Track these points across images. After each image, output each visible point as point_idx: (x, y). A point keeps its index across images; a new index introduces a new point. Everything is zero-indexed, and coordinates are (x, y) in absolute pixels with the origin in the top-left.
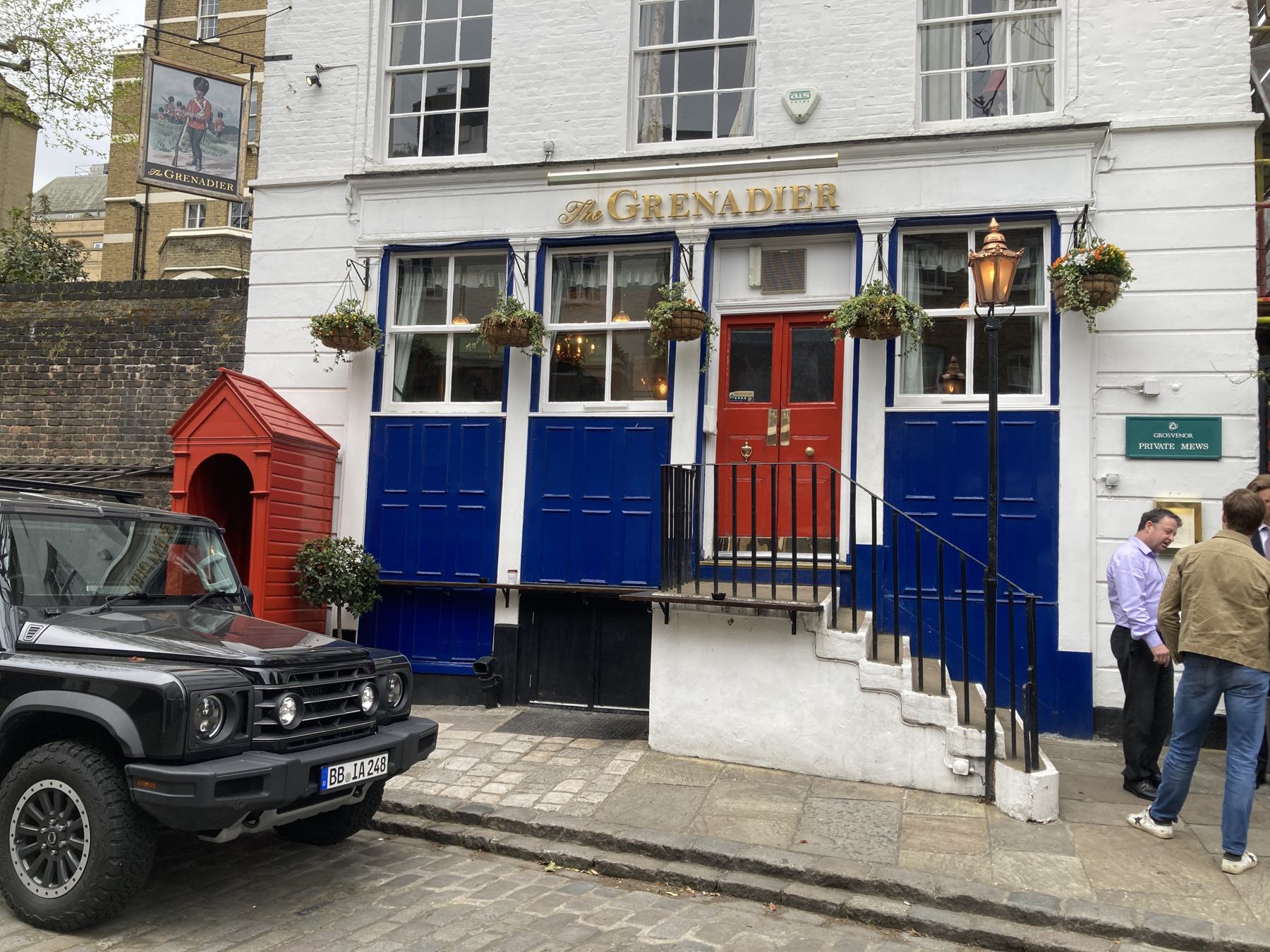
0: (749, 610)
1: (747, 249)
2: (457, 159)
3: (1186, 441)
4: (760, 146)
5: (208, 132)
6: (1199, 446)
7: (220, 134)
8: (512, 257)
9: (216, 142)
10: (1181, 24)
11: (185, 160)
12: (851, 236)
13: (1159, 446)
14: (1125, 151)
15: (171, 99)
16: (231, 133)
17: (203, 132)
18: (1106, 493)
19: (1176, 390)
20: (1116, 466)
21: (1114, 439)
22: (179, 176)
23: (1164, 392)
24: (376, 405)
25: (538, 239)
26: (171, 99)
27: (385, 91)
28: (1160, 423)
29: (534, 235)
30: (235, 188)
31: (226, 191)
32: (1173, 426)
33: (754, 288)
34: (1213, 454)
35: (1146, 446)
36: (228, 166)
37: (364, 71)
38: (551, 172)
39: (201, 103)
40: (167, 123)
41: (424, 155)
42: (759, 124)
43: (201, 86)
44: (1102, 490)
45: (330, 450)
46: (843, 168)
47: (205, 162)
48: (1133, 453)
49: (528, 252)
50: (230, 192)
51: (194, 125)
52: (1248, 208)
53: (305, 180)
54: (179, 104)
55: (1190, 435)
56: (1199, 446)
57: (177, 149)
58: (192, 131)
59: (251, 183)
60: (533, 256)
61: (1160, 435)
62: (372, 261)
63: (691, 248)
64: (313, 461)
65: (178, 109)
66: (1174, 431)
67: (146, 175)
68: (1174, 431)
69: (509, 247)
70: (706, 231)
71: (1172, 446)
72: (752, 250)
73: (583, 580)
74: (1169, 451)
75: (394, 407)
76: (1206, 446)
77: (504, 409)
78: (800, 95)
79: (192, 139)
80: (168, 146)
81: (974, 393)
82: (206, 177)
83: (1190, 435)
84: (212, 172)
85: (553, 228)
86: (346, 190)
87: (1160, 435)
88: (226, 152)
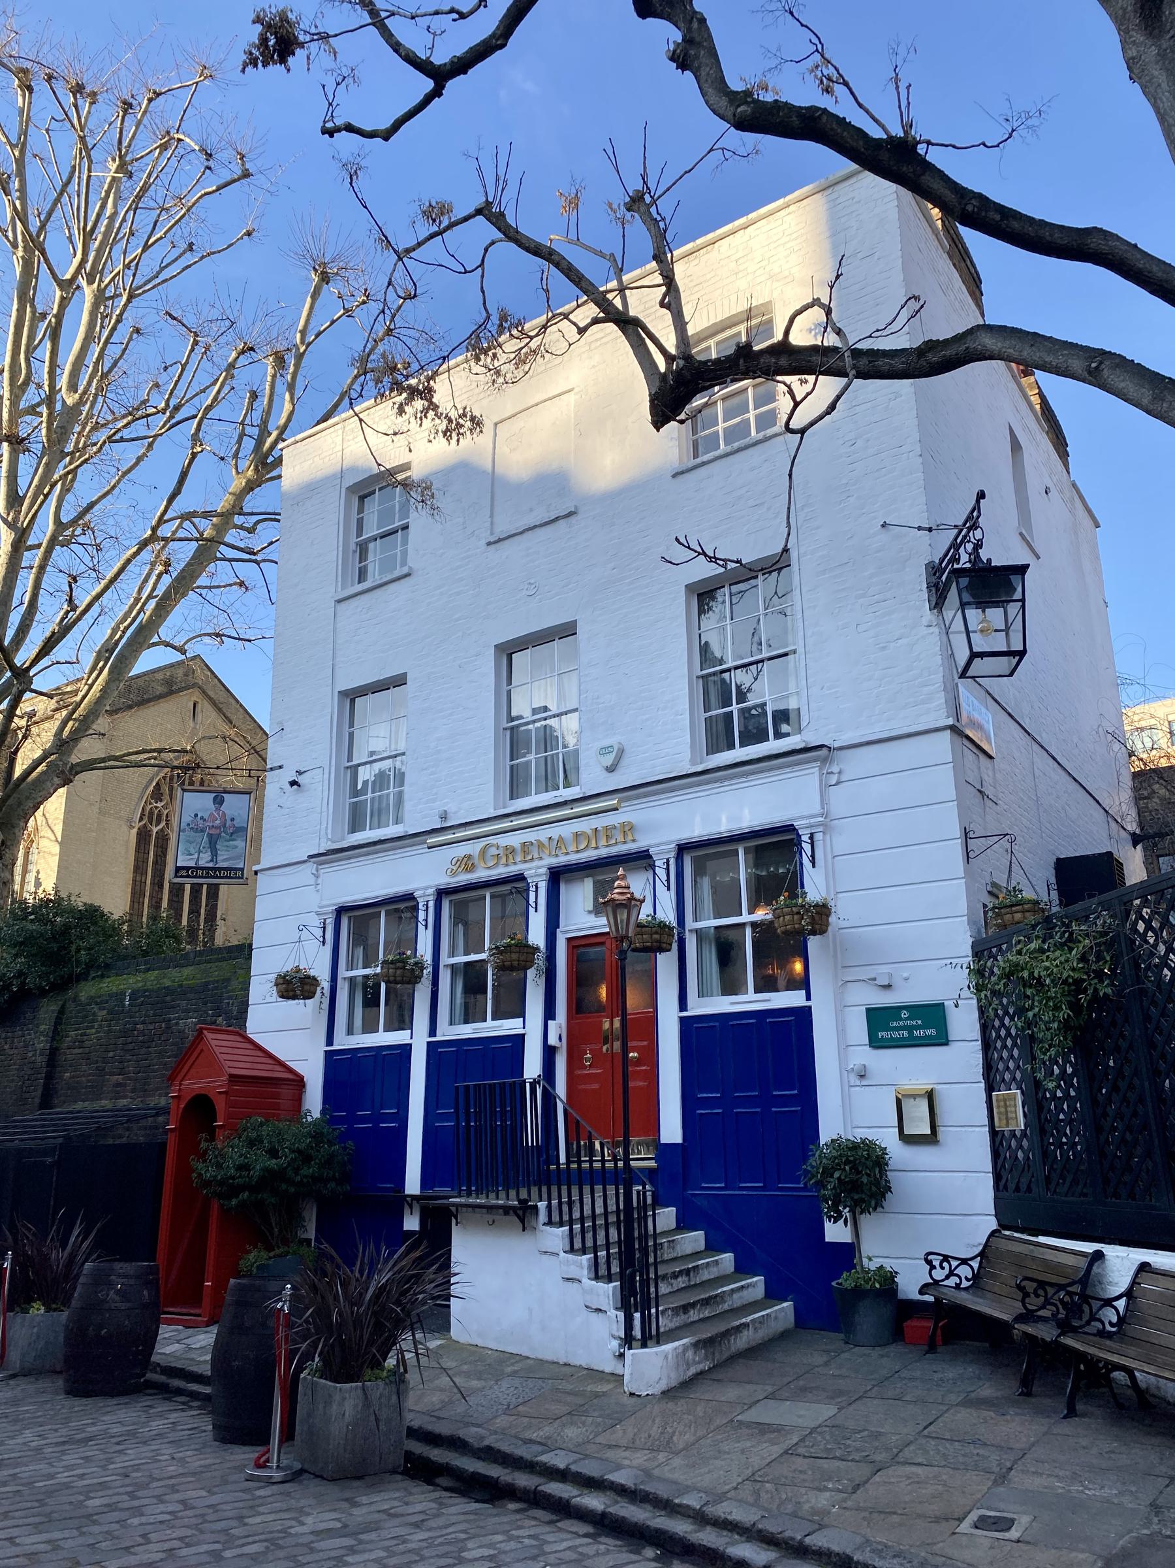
0: (501, 1211)
1: (582, 879)
2: (772, 746)
3: (918, 1027)
4: (581, 796)
5: (223, 834)
6: (928, 1032)
7: (232, 834)
8: (799, 842)
9: (229, 841)
10: (884, 648)
11: (205, 860)
12: (645, 862)
13: (895, 1034)
14: (853, 764)
15: (196, 815)
16: (240, 831)
17: (219, 835)
18: (858, 1083)
19: (906, 979)
20: (864, 1055)
21: (859, 1029)
22: (199, 873)
23: (897, 982)
24: (330, 1041)
25: (673, 846)
26: (196, 815)
27: (345, 780)
28: (893, 1012)
29: (431, 887)
30: (243, 874)
31: (236, 878)
32: (904, 1014)
33: (590, 912)
34: (942, 1040)
35: (884, 1034)
36: (237, 857)
37: (327, 771)
38: (430, 838)
39: (218, 814)
40: (192, 834)
41: (741, 746)
42: (584, 776)
43: (219, 801)
44: (854, 1080)
45: (298, 1083)
46: (625, 809)
47: (219, 858)
48: (875, 1043)
49: (325, 920)
50: (239, 878)
51: (213, 831)
52: (951, 804)
53: (287, 862)
54: (202, 818)
55: (919, 1022)
56: (928, 1032)
57: (199, 852)
58: (210, 836)
59: (255, 868)
60: (431, 904)
61: (895, 1024)
62: (328, 921)
63: (811, 838)
64: (286, 1092)
65: (201, 822)
66: (906, 1019)
67: (176, 876)
68: (906, 1019)
69: (415, 899)
70: (544, 870)
71: (906, 1034)
72: (586, 879)
73: (703, 1185)
74: (930, 1037)
75: (343, 1042)
76: (934, 1032)
77: (808, 998)
78: (605, 750)
79: (210, 843)
80: (192, 851)
81: (755, 992)
82: (220, 869)
83: (919, 1022)
84: (225, 865)
85: (445, 881)
86: (311, 867)
87: (895, 1024)
88: (236, 847)
